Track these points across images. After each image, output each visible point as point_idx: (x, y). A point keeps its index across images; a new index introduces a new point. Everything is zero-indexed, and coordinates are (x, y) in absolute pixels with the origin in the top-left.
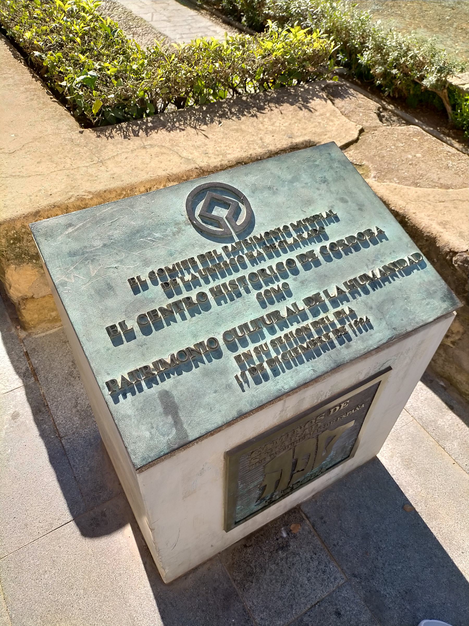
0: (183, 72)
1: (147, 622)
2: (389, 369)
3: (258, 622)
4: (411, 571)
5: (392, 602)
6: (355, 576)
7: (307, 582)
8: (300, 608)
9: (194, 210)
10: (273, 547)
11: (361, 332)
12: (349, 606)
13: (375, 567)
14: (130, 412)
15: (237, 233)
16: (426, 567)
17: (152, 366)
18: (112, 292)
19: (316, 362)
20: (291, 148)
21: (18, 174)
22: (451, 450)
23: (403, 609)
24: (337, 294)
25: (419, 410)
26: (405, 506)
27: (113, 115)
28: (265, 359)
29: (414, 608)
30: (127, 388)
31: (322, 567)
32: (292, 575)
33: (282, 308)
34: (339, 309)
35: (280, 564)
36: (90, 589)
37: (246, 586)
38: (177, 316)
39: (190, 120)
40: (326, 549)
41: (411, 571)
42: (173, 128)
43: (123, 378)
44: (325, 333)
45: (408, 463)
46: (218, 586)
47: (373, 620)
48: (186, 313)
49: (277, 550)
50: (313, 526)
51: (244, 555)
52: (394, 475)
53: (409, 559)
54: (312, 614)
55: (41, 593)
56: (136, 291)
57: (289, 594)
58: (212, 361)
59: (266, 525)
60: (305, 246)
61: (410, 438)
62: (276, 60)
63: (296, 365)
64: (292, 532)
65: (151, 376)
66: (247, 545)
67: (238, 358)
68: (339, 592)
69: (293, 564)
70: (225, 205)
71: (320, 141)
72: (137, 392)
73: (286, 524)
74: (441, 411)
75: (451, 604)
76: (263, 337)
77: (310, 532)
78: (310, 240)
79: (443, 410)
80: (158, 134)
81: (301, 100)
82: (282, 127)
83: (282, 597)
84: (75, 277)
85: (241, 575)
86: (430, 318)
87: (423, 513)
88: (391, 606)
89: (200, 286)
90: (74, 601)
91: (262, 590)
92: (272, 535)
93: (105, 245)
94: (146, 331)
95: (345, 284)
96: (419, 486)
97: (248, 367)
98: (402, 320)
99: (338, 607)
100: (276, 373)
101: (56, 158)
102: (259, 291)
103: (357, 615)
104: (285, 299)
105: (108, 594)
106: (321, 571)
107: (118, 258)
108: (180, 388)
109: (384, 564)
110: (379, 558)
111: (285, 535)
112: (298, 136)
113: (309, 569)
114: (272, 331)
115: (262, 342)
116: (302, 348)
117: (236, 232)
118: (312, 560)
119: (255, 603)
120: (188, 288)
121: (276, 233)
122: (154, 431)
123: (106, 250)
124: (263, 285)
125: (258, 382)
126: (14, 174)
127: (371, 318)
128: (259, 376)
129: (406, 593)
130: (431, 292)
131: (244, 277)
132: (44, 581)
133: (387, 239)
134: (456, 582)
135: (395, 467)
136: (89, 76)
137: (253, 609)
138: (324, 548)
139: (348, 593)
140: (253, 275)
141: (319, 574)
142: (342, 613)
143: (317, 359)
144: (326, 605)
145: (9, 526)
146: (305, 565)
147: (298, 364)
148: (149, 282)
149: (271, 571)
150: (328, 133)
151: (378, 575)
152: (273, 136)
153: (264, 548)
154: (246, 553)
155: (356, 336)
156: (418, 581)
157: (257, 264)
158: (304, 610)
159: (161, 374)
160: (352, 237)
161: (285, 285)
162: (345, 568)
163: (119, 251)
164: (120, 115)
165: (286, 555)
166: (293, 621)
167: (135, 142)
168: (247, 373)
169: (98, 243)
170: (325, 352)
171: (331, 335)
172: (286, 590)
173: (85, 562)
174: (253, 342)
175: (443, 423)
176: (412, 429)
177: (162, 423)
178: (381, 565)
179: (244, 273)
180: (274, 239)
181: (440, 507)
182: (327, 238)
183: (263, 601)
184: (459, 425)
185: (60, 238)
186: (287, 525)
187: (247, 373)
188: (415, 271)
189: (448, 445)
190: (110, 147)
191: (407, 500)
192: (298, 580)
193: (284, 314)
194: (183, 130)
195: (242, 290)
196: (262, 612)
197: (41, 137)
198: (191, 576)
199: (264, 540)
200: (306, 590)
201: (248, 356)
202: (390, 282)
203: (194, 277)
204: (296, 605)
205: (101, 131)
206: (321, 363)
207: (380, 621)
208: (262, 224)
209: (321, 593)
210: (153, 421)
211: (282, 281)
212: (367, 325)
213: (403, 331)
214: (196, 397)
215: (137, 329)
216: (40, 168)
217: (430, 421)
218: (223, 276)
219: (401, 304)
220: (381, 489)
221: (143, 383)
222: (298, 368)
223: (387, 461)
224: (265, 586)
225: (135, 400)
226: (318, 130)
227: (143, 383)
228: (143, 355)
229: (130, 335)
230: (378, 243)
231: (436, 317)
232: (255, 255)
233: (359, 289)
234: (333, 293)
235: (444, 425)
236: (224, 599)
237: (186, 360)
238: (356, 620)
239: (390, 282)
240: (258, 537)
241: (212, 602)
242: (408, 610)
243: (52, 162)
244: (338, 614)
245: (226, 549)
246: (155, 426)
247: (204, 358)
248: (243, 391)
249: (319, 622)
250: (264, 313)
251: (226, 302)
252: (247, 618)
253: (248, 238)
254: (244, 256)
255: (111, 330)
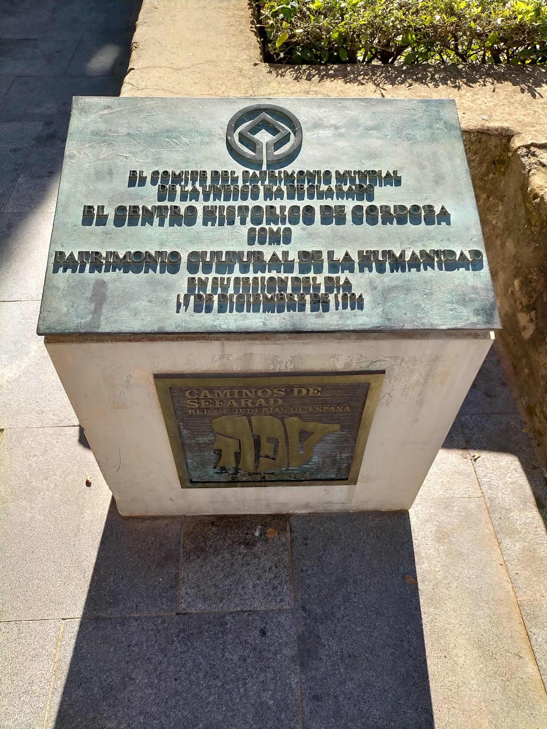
0: (393, 19)
1: (88, 539)
2: (383, 372)
3: (182, 594)
4: (369, 639)
5: (327, 655)
6: (304, 610)
7: (251, 587)
8: (229, 606)
9: (237, 126)
10: (238, 538)
11: (345, 307)
12: (279, 632)
13: (332, 614)
14: (61, 285)
15: (269, 163)
16: (389, 646)
17: (104, 255)
18: (108, 178)
19: (272, 317)
20: (478, 132)
21: (170, 88)
22: (508, 549)
23: (335, 669)
24: (341, 259)
25: (497, 490)
26: (407, 576)
27: (300, 54)
28: (219, 291)
29: (348, 675)
30: (71, 264)
31: (276, 583)
32: (241, 573)
33: (268, 251)
34: (334, 276)
35: (235, 557)
36: (60, 487)
37: (191, 558)
38: (156, 220)
39: (378, 77)
40: (291, 569)
41: (369, 639)
42: (355, 80)
43: (72, 255)
44: (302, 292)
45: (441, 536)
46: (166, 544)
47: (295, 659)
48: (167, 221)
49: (240, 543)
50: (292, 541)
51: (206, 530)
52: (416, 539)
53: (375, 627)
54: (237, 618)
55: (22, 470)
56: (132, 183)
57: (226, 588)
58: (164, 272)
59: (245, 516)
60: (338, 199)
61: (463, 514)
62: (521, 25)
63: (248, 311)
64: (266, 535)
65: (98, 263)
66: (215, 524)
67: (191, 281)
68: (277, 613)
69: (248, 564)
70: (274, 130)
71: (521, 132)
72: (78, 272)
73: (265, 526)
74: (525, 502)
75: (394, 696)
76: (231, 271)
77: (284, 545)
78: (350, 194)
79: (528, 504)
80: (332, 83)
81: (531, 81)
82: (482, 106)
83: (218, 586)
84: (85, 153)
85: (193, 546)
86: (445, 325)
87: (424, 594)
88: (324, 658)
89: (197, 200)
90: (43, 490)
91: (203, 569)
92: (245, 527)
93: (129, 134)
94: (119, 222)
95: (360, 253)
96: (439, 565)
97: (196, 292)
98: (406, 314)
99: (268, 627)
100: (222, 309)
101: (214, 83)
102: (255, 227)
103: (282, 645)
104: (279, 243)
105: (72, 499)
106: (272, 585)
107: (134, 149)
108: (118, 284)
109: (343, 617)
110: (342, 608)
111: (257, 534)
112: (495, 120)
113: (261, 577)
114: (244, 269)
115: (226, 276)
116: (265, 297)
117: (267, 161)
118: (269, 571)
119: (190, 577)
120: (184, 198)
121: (311, 176)
122: (71, 310)
123: (127, 138)
124: (264, 221)
125: (197, 309)
126: (166, 88)
127: (367, 299)
128: (203, 305)
129: (350, 656)
130: (467, 299)
131: (247, 208)
132: (30, 462)
133: (449, 223)
134: (416, 679)
135: (423, 533)
136: (289, 7)
137: (184, 580)
138: (289, 567)
139: (286, 620)
140: (258, 209)
141: (268, 587)
142: (268, 634)
143: (276, 314)
144: (257, 618)
145: (29, 406)
146: (259, 571)
147: (251, 311)
148: (149, 180)
149: (222, 558)
150: (537, 125)
151: (329, 622)
152: (464, 113)
153: (229, 535)
154: (210, 530)
155: (337, 309)
156: (371, 654)
157: (271, 199)
158: (231, 610)
159: (108, 264)
160: (403, 208)
161: (288, 230)
162: (299, 597)
163: (139, 143)
164: (308, 56)
165: (247, 553)
166: (215, 613)
167: (304, 84)
168: (192, 298)
169: (124, 130)
170: (288, 311)
171: (308, 297)
172: (226, 583)
173: (70, 464)
174: (217, 272)
175: (518, 518)
176: (472, 505)
177: (83, 306)
178: (339, 615)
179: (250, 203)
180: (306, 181)
181: (450, 598)
182: (371, 198)
183: (198, 579)
184: (538, 529)
185: (92, 116)
186: (265, 527)
187: (192, 298)
188: (462, 270)
189: (507, 542)
190: (274, 84)
191: (415, 571)
192: (244, 580)
193: (267, 257)
194: (363, 84)
195: (238, 219)
196: (191, 588)
197: (214, 61)
198: (148, 522)
199: (234, 527)
200: (245, 594)
201: (203, 284)
202: (419, 270)
203: (195, 190)
204: (227, 601)
205: (276, 68)
206: (276, 320)
207: (302, 664)
208: (303, 162)
209: (258, 605)
210: (76, 301)
211: (288, 225)
212: (358, 303)
213: (397, 326)
214: (128, 297)
215: (111, 218)
216: (193, 88)
217: (502, 508)
218: (227, 199)
219: (417, 297)
220: (391, 546)
221: (88, 266)
222: (249, 314)
223: (418, 522)
224: (209, 568)
225: (72, 277)
226: (528, 120)
227: (88, 266)
228: (103, 242)
229: (102, 220)
230: (434, 224)
231: (453, 327)
232: (275, 188)
233: (374, 264)
234: (339, 256)
235: (517, 520)
236: (164, 558)
237: (138, 262)
238: (278, 649)
239: (419, 270)
240: (229, 522)
241: (152, 554)
242: (340, 672)
243: (208, 85)
244: (263, 633)
245: (193, 517)
246: (75, 306)
247: (158, 267)
248: (178, 312)
249: (239, 628)
250: (247, 249)
251: (213, 225)
252: (174, 585)
253: (277, 171)
254: (262, 188)
255: (88, 210)
